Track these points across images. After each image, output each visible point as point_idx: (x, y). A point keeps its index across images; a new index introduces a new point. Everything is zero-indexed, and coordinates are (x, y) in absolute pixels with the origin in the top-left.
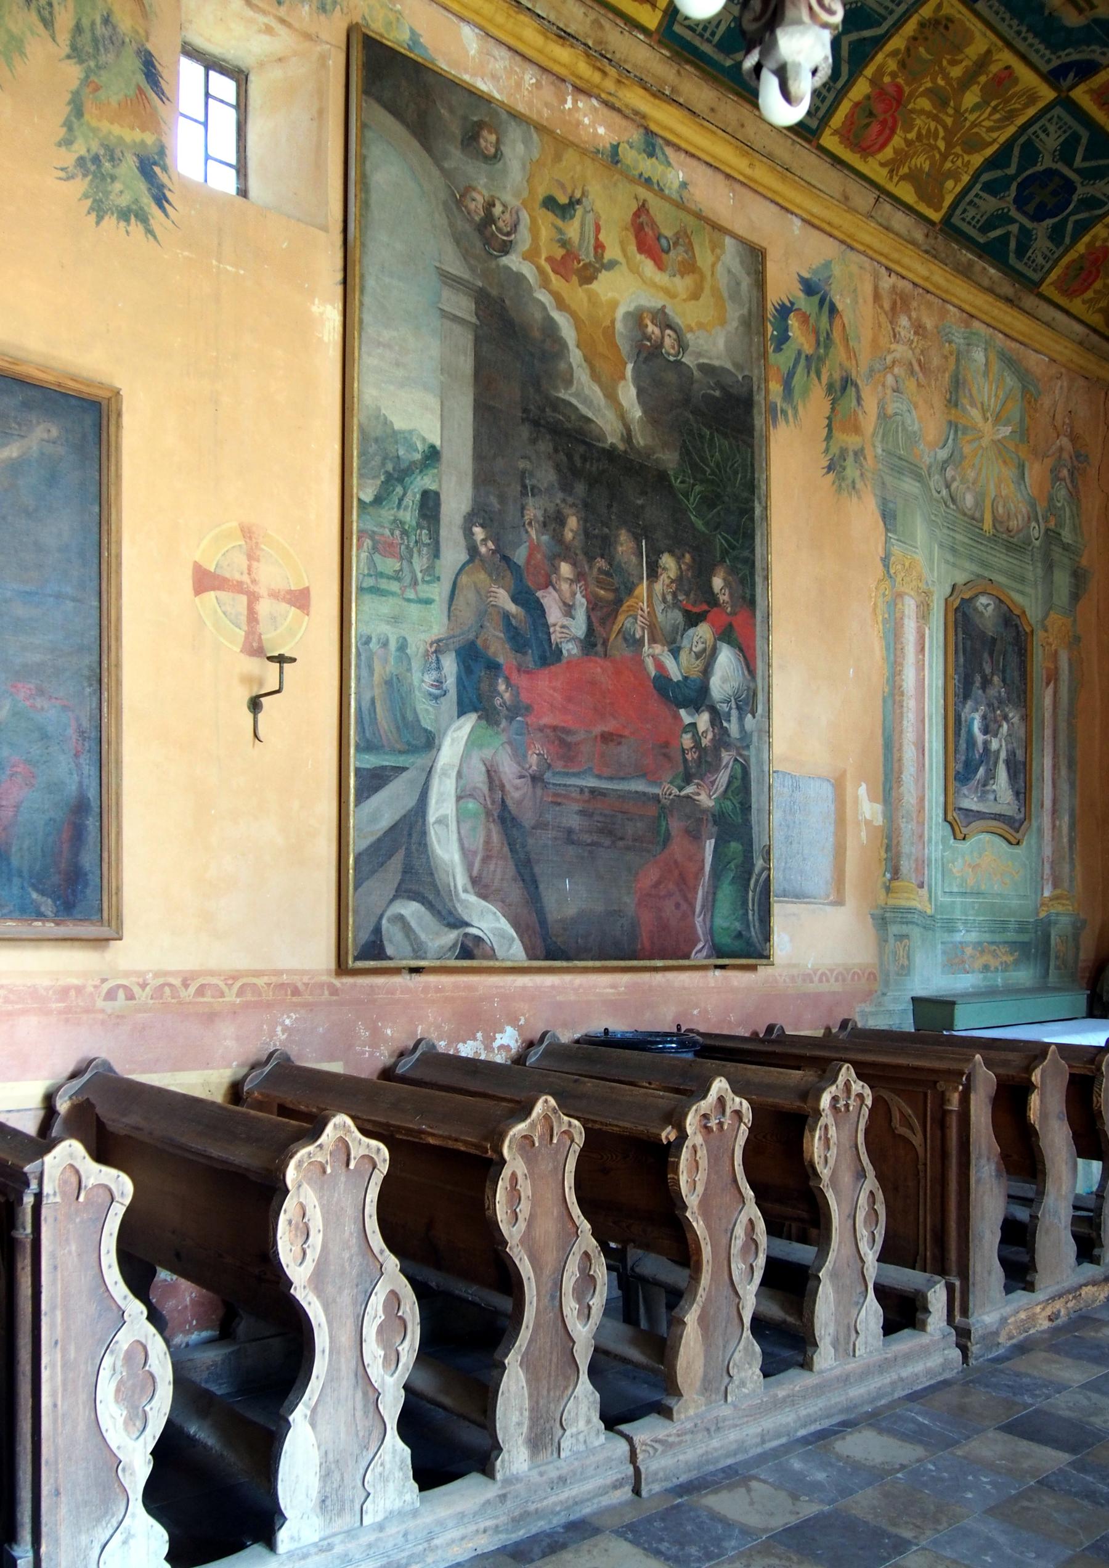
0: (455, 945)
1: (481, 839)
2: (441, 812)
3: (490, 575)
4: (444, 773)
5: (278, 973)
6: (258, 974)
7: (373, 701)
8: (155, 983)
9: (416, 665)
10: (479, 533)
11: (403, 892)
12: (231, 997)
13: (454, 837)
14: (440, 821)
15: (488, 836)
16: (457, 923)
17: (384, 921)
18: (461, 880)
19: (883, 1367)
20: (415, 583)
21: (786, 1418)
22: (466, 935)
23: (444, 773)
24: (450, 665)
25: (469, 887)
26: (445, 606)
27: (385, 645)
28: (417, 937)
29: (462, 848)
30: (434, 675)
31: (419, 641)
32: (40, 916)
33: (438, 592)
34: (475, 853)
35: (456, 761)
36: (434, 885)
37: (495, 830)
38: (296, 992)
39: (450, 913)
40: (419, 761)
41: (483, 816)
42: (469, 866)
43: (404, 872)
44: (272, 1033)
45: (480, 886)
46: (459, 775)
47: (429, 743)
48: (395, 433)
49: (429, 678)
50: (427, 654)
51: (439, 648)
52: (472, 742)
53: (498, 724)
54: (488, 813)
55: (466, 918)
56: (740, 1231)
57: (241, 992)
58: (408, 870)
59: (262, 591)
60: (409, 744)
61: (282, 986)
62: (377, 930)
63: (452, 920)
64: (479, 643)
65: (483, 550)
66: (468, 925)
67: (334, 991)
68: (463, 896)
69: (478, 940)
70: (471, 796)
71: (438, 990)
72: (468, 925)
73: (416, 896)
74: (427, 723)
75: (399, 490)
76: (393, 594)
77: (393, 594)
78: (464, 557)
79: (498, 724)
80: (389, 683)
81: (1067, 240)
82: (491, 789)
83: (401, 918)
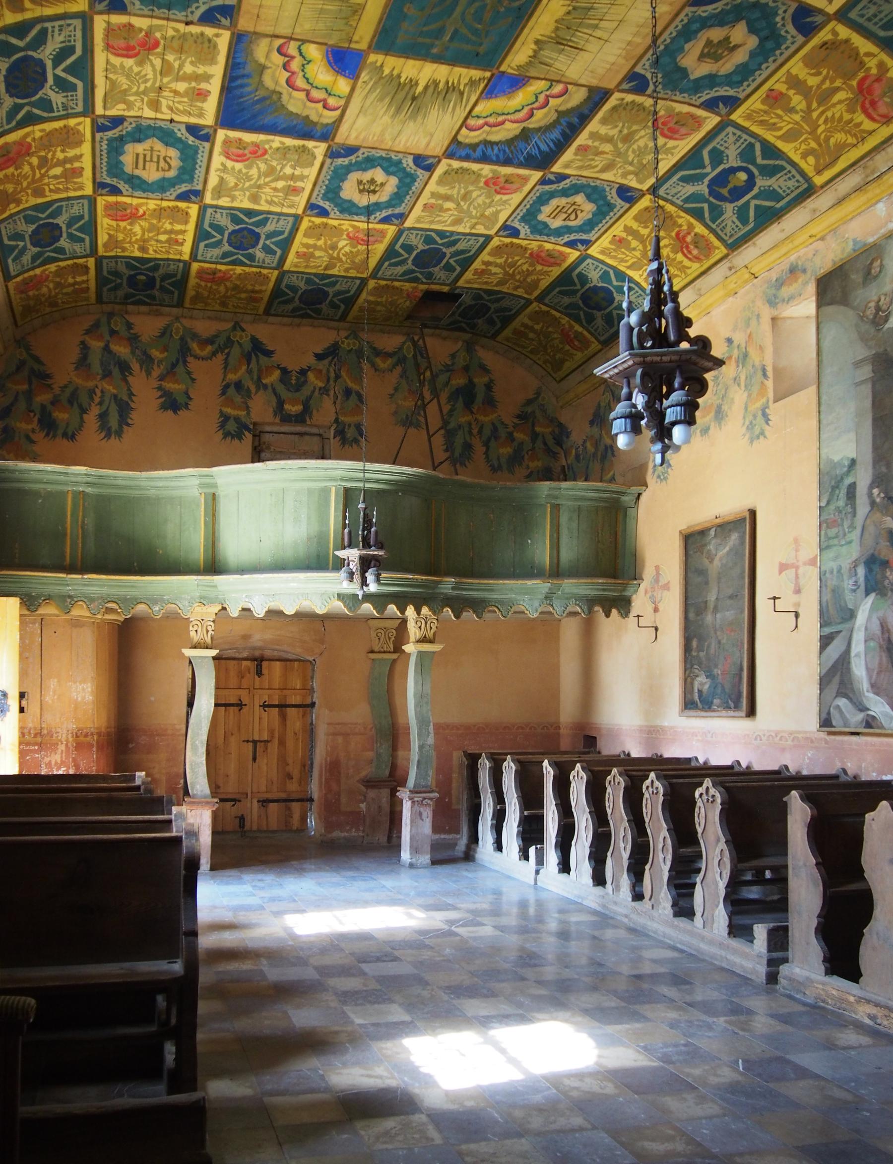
0: (862, 722)
1: (877, 662)
2: (858, 650)
3: (882, 512)
4: (859, 630)
5: (806, 732)
6: (799, 732)
7: (827, 601)
8: (767, 734)
9: (845, 577)
10: (876, 491)
11: (840, 694)
12: (790, 742)
13: (863, 662)
14: (857, 655)
15: (881, 659)
16: (863, 709)
17: (832, 709)
18: (865, 685)
19: (721, 945)
20: (845, 535)
21: (670, 931)
22: (868, 715)
23: (859, 630)
24: (861, 571)
25: (870, 689)
26: (858, 541)
27: (832, 572)
28: (845, 717)
29: (867, 669)
30: (854, 579)
31: (846, 564)
32: (730, 708)
33: (855, 535)
34: (873, 670)
35: (865, 622)
36: (853, 690)
37: (884, 655)
38: (812, 742)
39: (861, 704)
40: (847, 626)
41: (878, 649)
42: (870, 677)
43: (840, 684)
44: (804, 760)
45: (876, 688)
46: (866, 629)
47: (851, 615)
48: (835, 464)
49: (851, 582)
50: (850, 570)
51: (855, 564)
52: (873, 609)
53: (886, 595)
54: (881, 647)
55: (868, 706)
56: (661, 840)
57: (793, 740)
58: (842, 683)
59: (800, 563)
60: (842, 618)
61: (807, 738)
62: (829, 713)
63: (861, 707)
64: (876, 553)
65: (878, 500)
66: (869, 709)
67: (826, 742)
68: (867, 694)
69: (874, 717)
70: (872, 639)
71: (872, 745)
72: (869, 709)
73: (846, 696)
74: (850, 606)
75: (837, 492)
76: (835, 545)
77: (835, 545)
78: (868, 509)
79: (886, 595)
80: (833, 591)
81: (38, 27)
82: (883, 633)
83: (838, 707)
